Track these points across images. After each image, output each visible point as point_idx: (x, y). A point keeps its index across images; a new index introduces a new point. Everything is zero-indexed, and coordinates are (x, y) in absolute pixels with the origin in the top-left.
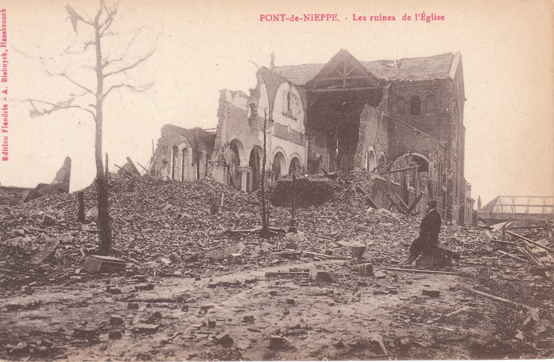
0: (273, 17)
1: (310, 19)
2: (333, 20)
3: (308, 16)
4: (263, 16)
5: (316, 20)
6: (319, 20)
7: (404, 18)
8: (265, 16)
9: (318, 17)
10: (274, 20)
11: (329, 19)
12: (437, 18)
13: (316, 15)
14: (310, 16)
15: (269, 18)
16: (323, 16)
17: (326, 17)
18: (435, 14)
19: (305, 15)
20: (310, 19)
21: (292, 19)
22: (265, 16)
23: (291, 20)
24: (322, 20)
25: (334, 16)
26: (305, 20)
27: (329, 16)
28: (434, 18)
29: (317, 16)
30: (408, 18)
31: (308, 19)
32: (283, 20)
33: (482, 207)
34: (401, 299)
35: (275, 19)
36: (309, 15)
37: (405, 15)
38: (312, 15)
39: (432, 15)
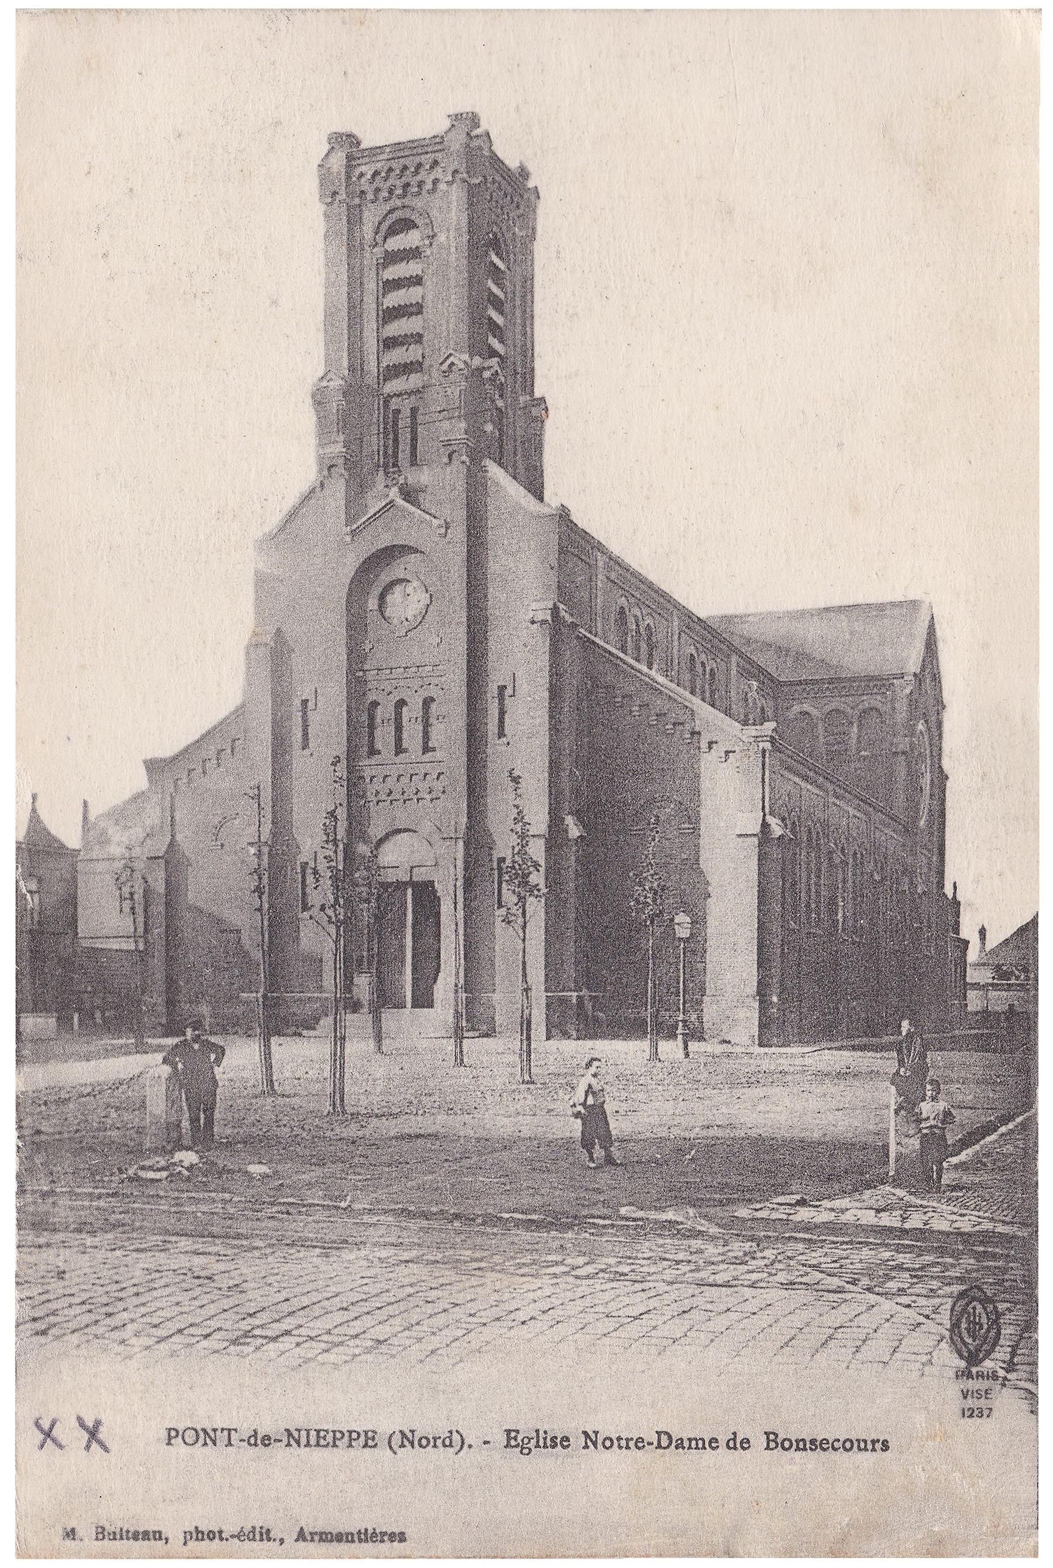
0: (202, 1434)
1: (303, 1441)
2: (366, 1445)
3: (296, 1434)
4: (173, 1433)
5: (318, 1445)
6: (326, 1446)
7: (731, 1444)
8: (779, 1447)
9: (324, 1438)
10: (205, 1444)
11: (354, 1443)
12: (549, 1443)
13: (318, 1431)
14: (304, 1433)
15: (190, 1436)
16: (338, 1435)
17: (362, 1438)
18: (545, 1432)
19: (585, 1433)
20: (303, 1441)
21: (252, 1441)
22: (779, 1447)
23: (249, 1444)
24: (335, 1445)
25: (322, 1434)
26: (289, 1445)
27: (354, 1435)
28: (541, 1443)
29: (513, 1434)
30: (742, 1443)
31: (298, 1443)
32: (230, 1444)
33: (988, 948)
34: (220, 1329)
35: (208, 1441)
36: (299, 1430)
37: (255, 1432)
38: (308, 1431)
39: (537, 1431)
